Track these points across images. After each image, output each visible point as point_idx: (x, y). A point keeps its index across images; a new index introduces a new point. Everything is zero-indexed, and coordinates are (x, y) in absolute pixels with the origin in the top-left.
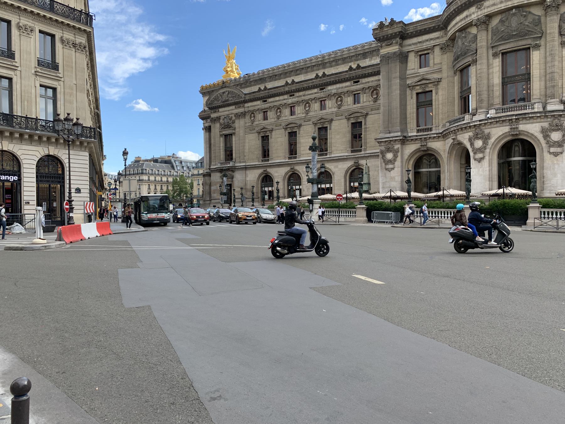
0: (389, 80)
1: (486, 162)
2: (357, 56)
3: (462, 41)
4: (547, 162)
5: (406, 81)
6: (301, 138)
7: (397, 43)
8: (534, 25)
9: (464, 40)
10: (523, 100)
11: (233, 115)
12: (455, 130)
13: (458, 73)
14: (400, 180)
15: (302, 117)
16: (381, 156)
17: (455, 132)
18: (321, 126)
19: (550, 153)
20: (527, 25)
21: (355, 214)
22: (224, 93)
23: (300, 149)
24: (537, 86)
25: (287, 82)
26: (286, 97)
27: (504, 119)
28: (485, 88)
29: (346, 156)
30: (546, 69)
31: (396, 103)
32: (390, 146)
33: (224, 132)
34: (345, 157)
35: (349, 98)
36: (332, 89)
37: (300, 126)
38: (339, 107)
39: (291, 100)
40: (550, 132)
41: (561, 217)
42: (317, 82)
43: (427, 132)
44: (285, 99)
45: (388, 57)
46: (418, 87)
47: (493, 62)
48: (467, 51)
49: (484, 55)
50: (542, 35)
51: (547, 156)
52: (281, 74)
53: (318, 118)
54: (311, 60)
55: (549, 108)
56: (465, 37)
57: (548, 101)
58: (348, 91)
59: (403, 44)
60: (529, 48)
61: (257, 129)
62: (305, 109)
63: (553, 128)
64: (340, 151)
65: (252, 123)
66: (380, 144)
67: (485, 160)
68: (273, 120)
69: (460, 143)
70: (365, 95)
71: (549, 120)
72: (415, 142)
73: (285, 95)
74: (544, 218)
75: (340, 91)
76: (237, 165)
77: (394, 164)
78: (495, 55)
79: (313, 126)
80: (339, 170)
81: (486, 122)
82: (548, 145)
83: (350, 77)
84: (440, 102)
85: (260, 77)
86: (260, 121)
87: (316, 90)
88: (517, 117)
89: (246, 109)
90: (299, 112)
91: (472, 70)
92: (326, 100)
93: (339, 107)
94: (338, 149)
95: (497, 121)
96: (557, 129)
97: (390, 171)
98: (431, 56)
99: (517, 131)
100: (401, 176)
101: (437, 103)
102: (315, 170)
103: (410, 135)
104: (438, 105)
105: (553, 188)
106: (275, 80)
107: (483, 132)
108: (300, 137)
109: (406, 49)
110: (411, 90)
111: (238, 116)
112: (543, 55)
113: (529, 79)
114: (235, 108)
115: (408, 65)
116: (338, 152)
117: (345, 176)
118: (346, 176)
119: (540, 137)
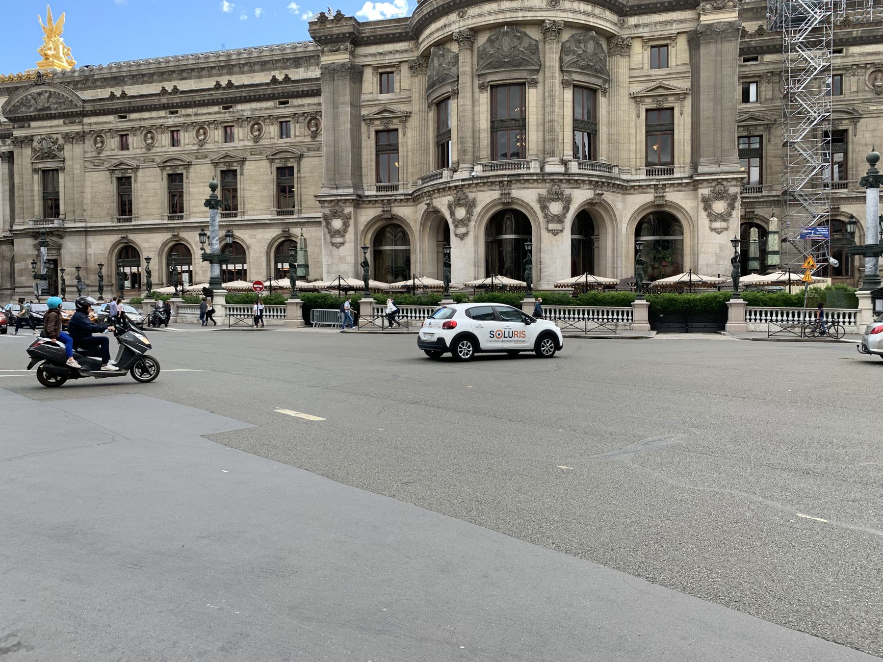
0: (335, 105)
1: (470, 239)
3: (439, 61)
5: (360, 110)
6: (191, 185)
7: (346, 49)
9: (442, 59)
10: (516, 155)
11: (59, 136)
14: (353, 261)
16: (324, 223)
17: (430, 194)
18: (225, 168)
19: (549, 231)
20: (522, 51)
21: (284, 313)
22: (39, 94)
23: (189, 204)
24: (533, 137)
26: (162, 113)
27: (494, 180)
31: (346, 143)
32: (338, 208)
33: (40, 166)
34: (268, 222)
35: (272, 127)
36: (245, 109)
37: (189, 165)
38: (257, 139)
39: (171, 121)
42: (218, 95)
44: (160, 118)
45: (334, 70)
46: (378, 122)
47: (479, 97)
48: (445, 76)
49: (468, 85)
50: (539, 68)
51: (545, 235)
52: (153, 74)
53: (220, 155)
55: (548, 169)
57: (547, 160)
60: (524, 84)
61: (108, 164)
62: (198, 138)
63: (552, 196)
65: (99, 153)
67: (469, 237)
68: (139, 151)
69: (437, 211)
70: (298, 125)
71: (547, 185)
73: (161, 110)
75: (257, 114)
76: (67, 225)
78: (482, 87)
79: (211, 167)
81: (471, 182)
83: (274, 94)
84: (410, 147)
85: (114, 75)
86: (114, 150)
87: (216, 109)
88: (509, 179)
89: (85, 127)
90: (187, 142)
91: (453, 104)
93: (257, 139)
94: (256, 208)
95: (484, 182)
96: (557, 199)
97: (338, 248)
98: (396, 77)
99: (509, 198)
101: (405, 149)
103: (366, 193)
106: (143, 83)
109: (360, 61)
111: (70, 138)
112: (541, 97)
114: (64, 123)
116: (255, 212)
117: (267, 252)
119: (537, 207)
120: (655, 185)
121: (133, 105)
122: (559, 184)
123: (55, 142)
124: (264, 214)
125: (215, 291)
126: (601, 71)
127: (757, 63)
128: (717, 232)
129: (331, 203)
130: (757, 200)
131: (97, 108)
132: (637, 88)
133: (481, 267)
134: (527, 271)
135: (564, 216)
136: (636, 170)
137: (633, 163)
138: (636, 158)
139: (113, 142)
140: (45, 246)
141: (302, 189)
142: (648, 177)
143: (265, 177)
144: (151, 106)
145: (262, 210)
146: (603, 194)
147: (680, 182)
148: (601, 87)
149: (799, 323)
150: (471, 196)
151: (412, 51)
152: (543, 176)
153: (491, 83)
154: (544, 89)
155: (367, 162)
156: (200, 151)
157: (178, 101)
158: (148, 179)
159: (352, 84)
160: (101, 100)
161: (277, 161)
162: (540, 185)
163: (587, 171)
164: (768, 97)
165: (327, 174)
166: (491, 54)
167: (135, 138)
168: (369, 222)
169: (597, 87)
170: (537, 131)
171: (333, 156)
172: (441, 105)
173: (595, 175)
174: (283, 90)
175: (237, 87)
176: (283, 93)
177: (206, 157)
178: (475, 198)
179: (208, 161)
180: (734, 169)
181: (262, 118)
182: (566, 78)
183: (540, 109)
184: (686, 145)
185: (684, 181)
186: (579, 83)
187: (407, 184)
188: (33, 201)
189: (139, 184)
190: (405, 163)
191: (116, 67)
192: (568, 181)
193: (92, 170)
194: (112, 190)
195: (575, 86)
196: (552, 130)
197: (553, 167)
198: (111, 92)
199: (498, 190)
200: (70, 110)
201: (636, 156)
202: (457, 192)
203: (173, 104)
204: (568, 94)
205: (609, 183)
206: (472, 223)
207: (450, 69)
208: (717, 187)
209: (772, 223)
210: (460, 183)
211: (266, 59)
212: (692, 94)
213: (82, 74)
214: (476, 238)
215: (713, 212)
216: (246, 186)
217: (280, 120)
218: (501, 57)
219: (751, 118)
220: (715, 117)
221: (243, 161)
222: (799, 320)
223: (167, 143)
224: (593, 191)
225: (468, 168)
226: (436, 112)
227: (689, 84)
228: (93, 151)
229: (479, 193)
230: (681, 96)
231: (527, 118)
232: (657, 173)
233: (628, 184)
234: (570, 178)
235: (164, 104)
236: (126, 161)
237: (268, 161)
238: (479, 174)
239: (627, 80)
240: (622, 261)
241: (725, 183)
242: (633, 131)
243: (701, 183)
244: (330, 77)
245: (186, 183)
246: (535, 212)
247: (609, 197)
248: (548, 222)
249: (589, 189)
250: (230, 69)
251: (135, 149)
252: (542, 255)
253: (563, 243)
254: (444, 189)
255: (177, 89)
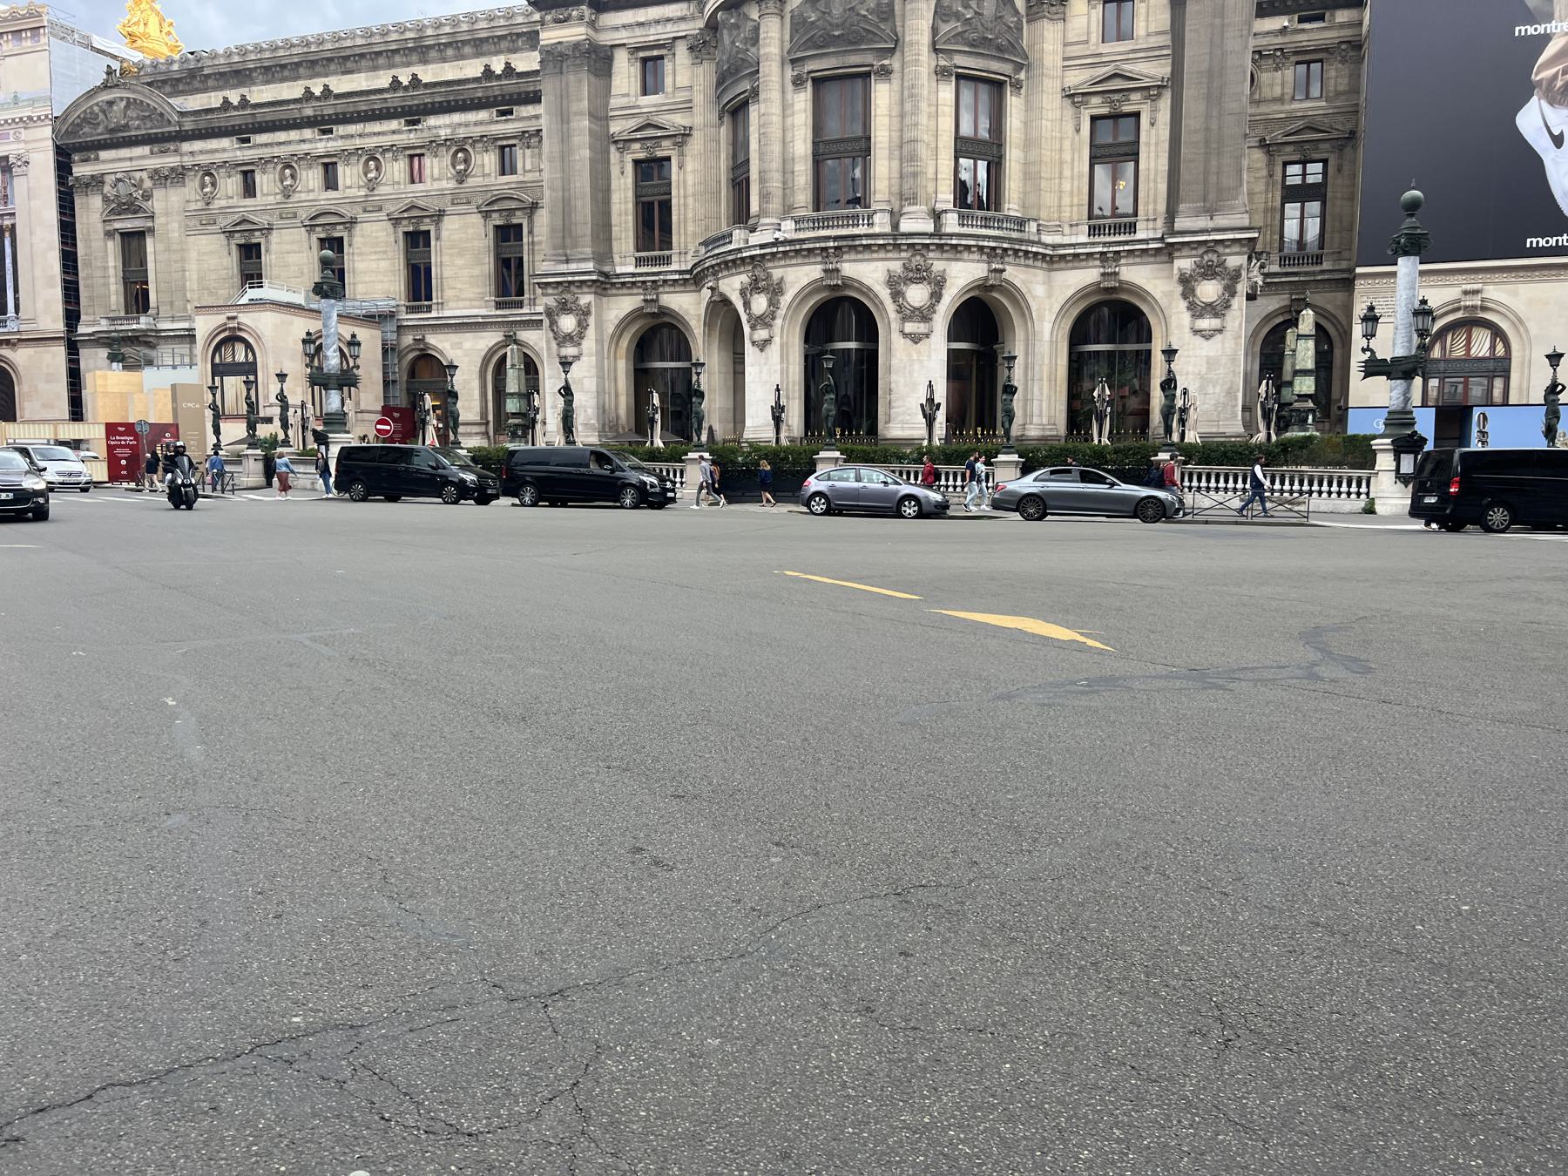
0: (563, 117)
1: (774, 350)
2: (514, 37)
3: (730, 35)
4: (898, 355)
5: (608, 126)
6: (356, 258)
7: (581, 18)
8: (878, 17)
9: (735, 33)
10: (856, 201)
11: (144, 175)
12: (712, 266)
13: (726, 119)
14: (594, 388)
15: (358, 197)
16: (546, 323)
17: (715, 271)
18: (411, 229)
19: (905, 335)
20: (865, 16)
21: (682, 477)
22: (111, 103)
24: (883, 169)
25: (487, 68)
26: (308, 133)
27: (811, 246)
28: (775, 164)
29: (483, 317)
30: (902, 130)
31: (582, 183)
32: (568, 296)
33: (117, 225)
34: (480, 320)
35: (486, 157)
36: (441, 125)
37: (353, 222)
38: (461, 177)
39: (323, 146)
40: (905, 284)
41: (1282, 489)
42: (395, 100)
43: (1099, 235)
44: (304, 141)
45: (561, 55)
46: (637, 146)
47: (793, 99)
48: (740, 62)
49: (774, 79)
50: (895, 45)
51: (898, 342)
52: (298, 65)
53: (402, 205)
54: (387, 33)
55: (905, 226)
56: (737, 26)
57: (905, 210)
58: (482, 136)
59: (601, 24)
60: (868, 74)
61: (224, 222)
62: (366, 176)
63: (911, 275)
64: (467, 303)
65: (208, 204)
66: (544, 291)
67: (773, 346)
68: (271, 199)
69: (726, 302)
70: (528, 152)
71: (903, 255)
72: (631, 291)
74: (1217, 489)
75: (462, 133)
76: (161, 326)
77: (579, 344)
78: (798, 82)
79: (388, 225)
80: (466, 356)
81: (775, 250)
82: (901, 315)
83: (488, 98)
84: (690, 190)
85: (235, 67)
86: (232, 198)
87: (394, 124)
88: (836, 244)
90: (348, 183)
91: (754, 111)
92: (423, 155)
93: (461, 177)
95: (795, 251)
96: (920, 278)
98: (668, 65)
99: (838, 279)
100: (598, 377)
101: (682, 191)
102: (332, 350)
103: (619, 270)
104: (685, 197)
105: (908, 418)
106: (283, 80)
107: (769, 276)
108: (353, 254)
109: (606, 39)
110: (621, 151)
111: (162, 178)
112: (896, 97)
113: (868, 151)
114: (152, 153)
115: (613, 83)
116: (461, 304)
117: (480, 371)
118: (486, 371)
119: (884, 294)
120: (1102, 253)
121: (258, 120)
122: (923, 252)
123: (138, 185)
124: (475, 307)
125: (330, 435)
126: (1010, 48)
127: (1322, 25)
128: (1203, 336)
129: (557, 288)
130: (1312, 278)
131: (202, 125)
132: (1077, 78)
133: (794, 398)
134: (825, 406)
135: (931, 309)
136: (1071, 226)
137: (1066, 215)
138: (1071, 206)
139: (231, 185)
140: (118, 362)
141: (536, 263)
142: (1092, 240)
143: (476, 243)
144: (288, 120)
145: (471, 300)
146: (1004, 270)
147: (1144, 247)
148: (1010, 77)
149: (1244, 493)
150: (776, 274)
151: (693, 18)
152: (895, 239)
153: (813, 75)
154: (903, 83)
155: (620, 215)
156: (370, 199)
157: (331, 112)
158: (288, 247)
159: (592, 78)
160: (467, 81)
161: (495, 215)
162: (890, 255)
163: (975, 229)
164: (1341, 88)
165: (551, 237)
166: (813, 23)
167: (265, 177)
168: (622, 321)
169: (1002, 78)
170: (890, 159)
171: (561, 205)
172: (736, 112)
173: (989, 237)
174: (502, 90)
175: (427, 85)
176: (503, 96)
177: (380, 209)
178: (782, 278)
179: (382, 215)
180: (1238, 223)
181: (470, 141)
182: (943, 63)
183: (896, 120)
184: (1159, 180)
185: (1151, 246)
186: (967, 71)
187: (686, 253)
188: (107, 285)
189: (274, 257)
190: (682, 217)
191: (239, 54)
192: (940, 247)
193: (197, 232)
194: (230, 266)
195: (959, 77)
196: (913, 158)
197: (916, 223)
198: (224, 98)
199: (820, 263)
200: (160, 130)
201: (1072, 201)
202: (754, 267)
203: (323, 116)
204: (947, 92)
205: (1016, 251)
206: (778, 322)
207: (747, 50)
208: (1206, 258)
209: (1303, 320)
210: (758, 252)
211: (483, 35)
212: (1172, 87)
213: (185, 66)
214: (784, 347)
215: (1197, 302)
216: (446, 259)
217: (500, 143)
218: (828, 28)
219: (1308, 128)
220: (1207, 129)
221: (439, 215)
222: (1244, 489)
223: (316, 185)
224: (986, 265)
225: (772, 224)
226: (730, 123)
227: (1168, 69)
228: (278, 194)
229: (789, 269)
230: (1152, 92)
231: (872, 135)
232: (1107, 231)
233: (1056, 253)
234: (943, 242)
235: (309, 117)
236: (252, 217)
237: (479, 215)
238: (790, 236)
239: (1060, 63)
240: (1041, 389)
241: (1220, 249)
242: (1067, 157)
243: (1179, 250)
244: (555, 67)
245: (348, 253)
246: (882, 303)
247: (1015, 274)
248: (904, 319)
249: (978, 261)
250: (423, 53)
251: (264, 195)
252: (894, 377)
253: (930, 356)
254: (734, 261)
255: (329, 90)
